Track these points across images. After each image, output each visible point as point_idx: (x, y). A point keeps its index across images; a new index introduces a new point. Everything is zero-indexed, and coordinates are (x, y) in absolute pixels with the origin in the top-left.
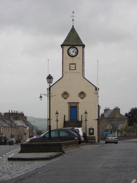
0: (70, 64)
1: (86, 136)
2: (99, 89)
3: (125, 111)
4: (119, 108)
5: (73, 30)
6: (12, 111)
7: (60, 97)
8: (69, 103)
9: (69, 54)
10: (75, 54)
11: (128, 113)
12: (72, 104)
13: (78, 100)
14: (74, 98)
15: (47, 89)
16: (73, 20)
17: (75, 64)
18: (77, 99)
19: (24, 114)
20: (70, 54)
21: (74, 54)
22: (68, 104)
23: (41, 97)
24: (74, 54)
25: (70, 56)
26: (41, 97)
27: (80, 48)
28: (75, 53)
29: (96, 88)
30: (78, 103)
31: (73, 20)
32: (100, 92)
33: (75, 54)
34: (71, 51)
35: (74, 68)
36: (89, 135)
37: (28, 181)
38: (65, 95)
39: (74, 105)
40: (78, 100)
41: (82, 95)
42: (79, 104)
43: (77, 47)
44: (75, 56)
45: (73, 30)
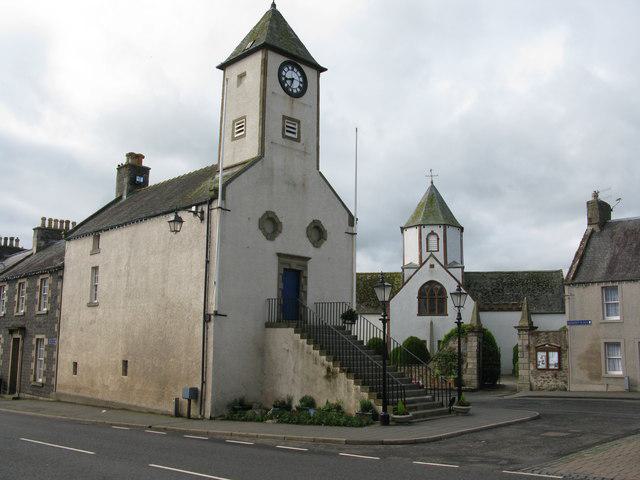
0: (284, 117)
4: (145, 163)
8: (279, 255)
17: (299, 122)
18: (301, 246)
22: (276, 260)
25: (286, 90)
27: (309, 72)
35: (295, 136)
38: (271, 225)
42: (310, 264)
43: (306, 69)
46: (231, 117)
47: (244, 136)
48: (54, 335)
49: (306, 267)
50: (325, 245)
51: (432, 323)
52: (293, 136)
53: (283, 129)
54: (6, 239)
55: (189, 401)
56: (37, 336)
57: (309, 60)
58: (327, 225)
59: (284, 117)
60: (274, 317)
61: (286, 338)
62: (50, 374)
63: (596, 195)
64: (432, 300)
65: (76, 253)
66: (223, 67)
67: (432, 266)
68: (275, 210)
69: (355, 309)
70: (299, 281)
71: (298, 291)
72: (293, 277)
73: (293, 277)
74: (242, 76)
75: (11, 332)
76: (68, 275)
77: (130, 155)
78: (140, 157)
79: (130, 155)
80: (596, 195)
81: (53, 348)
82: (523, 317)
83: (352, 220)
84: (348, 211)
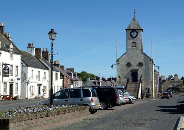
2: (153, 60)
3: (180, 78)
6: (2, 63)
9: (131, 36)
10: (136, 36)
11: (60, 65)
13: (138, 68)
14: (134, 67)
15: (116, 60)
17: (136, 43)
19: (104, 78)
21: (135, 35)
23: (112, 66)
24: (135, 35)
25: (132, 37)
26: (112, 66)
29: (151, 59)
31: (134, 12)
33: (136, 36)
34: (133, 33)
40: (131, 68)
41: (141, 64)
43: (137, 31)
44: (136, 37)
68: (130, 61)
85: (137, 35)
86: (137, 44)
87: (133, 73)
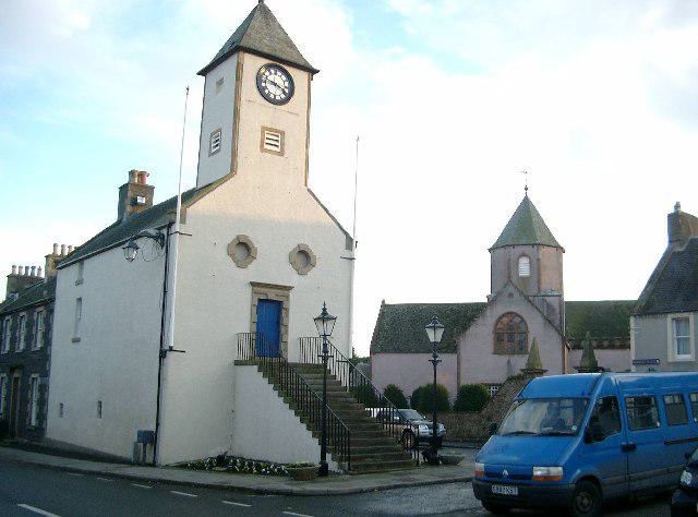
0: (264, 129)
1: (527, 369)
4: (148, 182)
5: (526, 201)
7: (221, 254)
8: (253, 284)
9: (261, 90)
12: (266, 290)
14: (272, 267)
16: (526, 189)
17: (283, 133)
18: (282, 274)
20: (267, 91)
21: (280, 95)
22: (249, 290)
24: (280, 95)
25: (266, 98)
27: (299, 77)
28: (284, 92)
30: (290, 288)
31: (526, 189)
32: (358, 252)
35: (278, 150)
36: (687, 320)
37: (467, 425)
38: (243, 249)
39: (272, 295)
42: (292, 294)
45: (526, 201)
46: (209, 131)
47: (218, 151)
48: (45, 374)
49: (288, 297)
50: (313, 272)
51: (509, 361)
52: (276, 149)
53: (262, 142)
54: (27, 268)
55: (145, 445)
56: (33, 376)
57: (302, 63)
58: (315, 251)
59: (264, 129)
60: (251, 358)
61: (253, 378)
62: (42, 417)
63: (677, 206)
64: (510, 337)
65: (66, 279)
66: (203, 73)
67: (511, 295)
69: (632, 320)
70: (280, 312)
71: (278, 323)
72: (270, 310)
73: (270, 310)
74: (220, 83)
75: (12, 370)
76: (59, 307)
77: (132, 173)
78: (142, 175)
79: (132, 173)
80: (677, 206)
81: (44, 389)
82: (584, 356)
83: (350, 243)
84: (346, 233)
85: (292, 93)
86: (289, 141)
87: (260, 300)
